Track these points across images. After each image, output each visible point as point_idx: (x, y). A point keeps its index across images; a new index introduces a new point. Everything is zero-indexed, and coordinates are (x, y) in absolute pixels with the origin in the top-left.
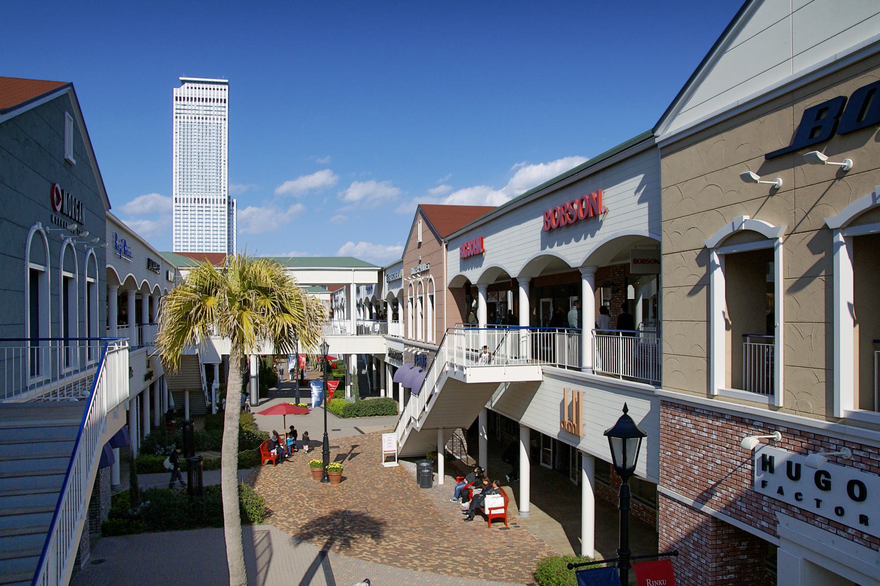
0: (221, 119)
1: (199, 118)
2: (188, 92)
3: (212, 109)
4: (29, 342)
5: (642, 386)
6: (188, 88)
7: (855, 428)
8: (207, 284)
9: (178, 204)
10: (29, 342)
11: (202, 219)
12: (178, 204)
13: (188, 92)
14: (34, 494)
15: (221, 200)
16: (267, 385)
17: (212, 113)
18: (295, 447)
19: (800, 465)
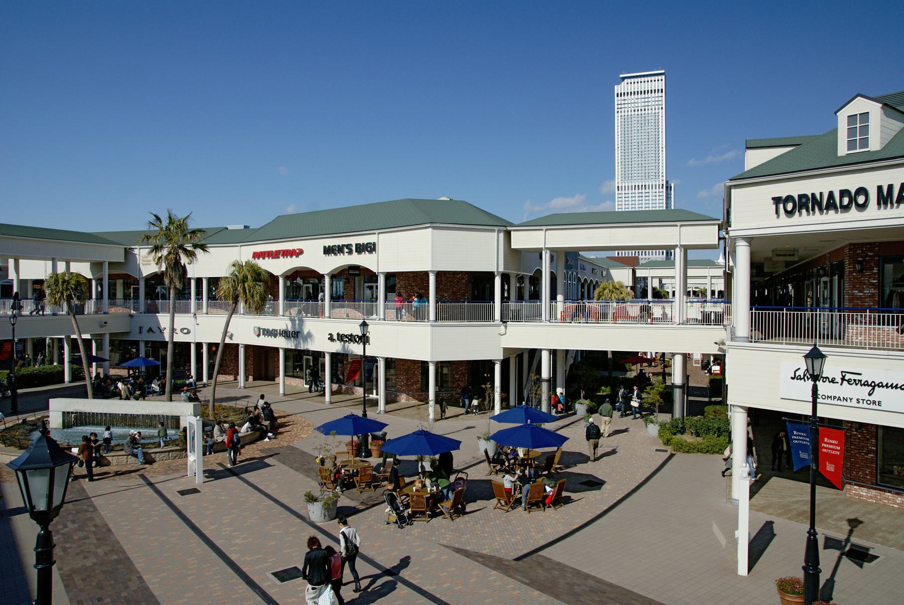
2: (628, 87)
13: (628, 87)
17: (650, 104)
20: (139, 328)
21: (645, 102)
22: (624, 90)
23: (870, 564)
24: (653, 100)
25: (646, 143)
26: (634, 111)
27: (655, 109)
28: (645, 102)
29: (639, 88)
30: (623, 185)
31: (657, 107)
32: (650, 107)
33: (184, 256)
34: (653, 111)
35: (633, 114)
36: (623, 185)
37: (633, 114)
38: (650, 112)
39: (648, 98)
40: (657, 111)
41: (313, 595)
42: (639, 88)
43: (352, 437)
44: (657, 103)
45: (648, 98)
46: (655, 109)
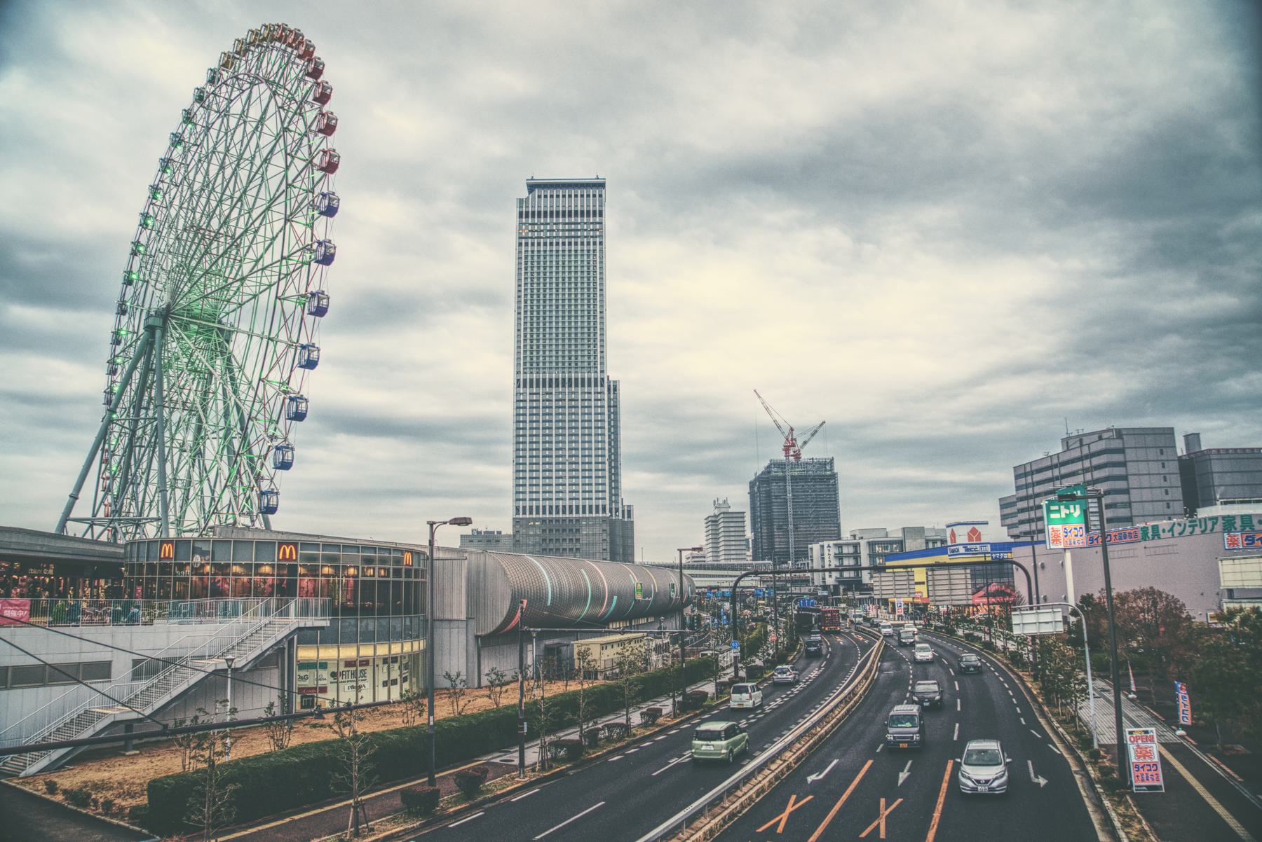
0: (595, 243)
6: (539, 197)
31: (592, 240)
32: (579, 240)
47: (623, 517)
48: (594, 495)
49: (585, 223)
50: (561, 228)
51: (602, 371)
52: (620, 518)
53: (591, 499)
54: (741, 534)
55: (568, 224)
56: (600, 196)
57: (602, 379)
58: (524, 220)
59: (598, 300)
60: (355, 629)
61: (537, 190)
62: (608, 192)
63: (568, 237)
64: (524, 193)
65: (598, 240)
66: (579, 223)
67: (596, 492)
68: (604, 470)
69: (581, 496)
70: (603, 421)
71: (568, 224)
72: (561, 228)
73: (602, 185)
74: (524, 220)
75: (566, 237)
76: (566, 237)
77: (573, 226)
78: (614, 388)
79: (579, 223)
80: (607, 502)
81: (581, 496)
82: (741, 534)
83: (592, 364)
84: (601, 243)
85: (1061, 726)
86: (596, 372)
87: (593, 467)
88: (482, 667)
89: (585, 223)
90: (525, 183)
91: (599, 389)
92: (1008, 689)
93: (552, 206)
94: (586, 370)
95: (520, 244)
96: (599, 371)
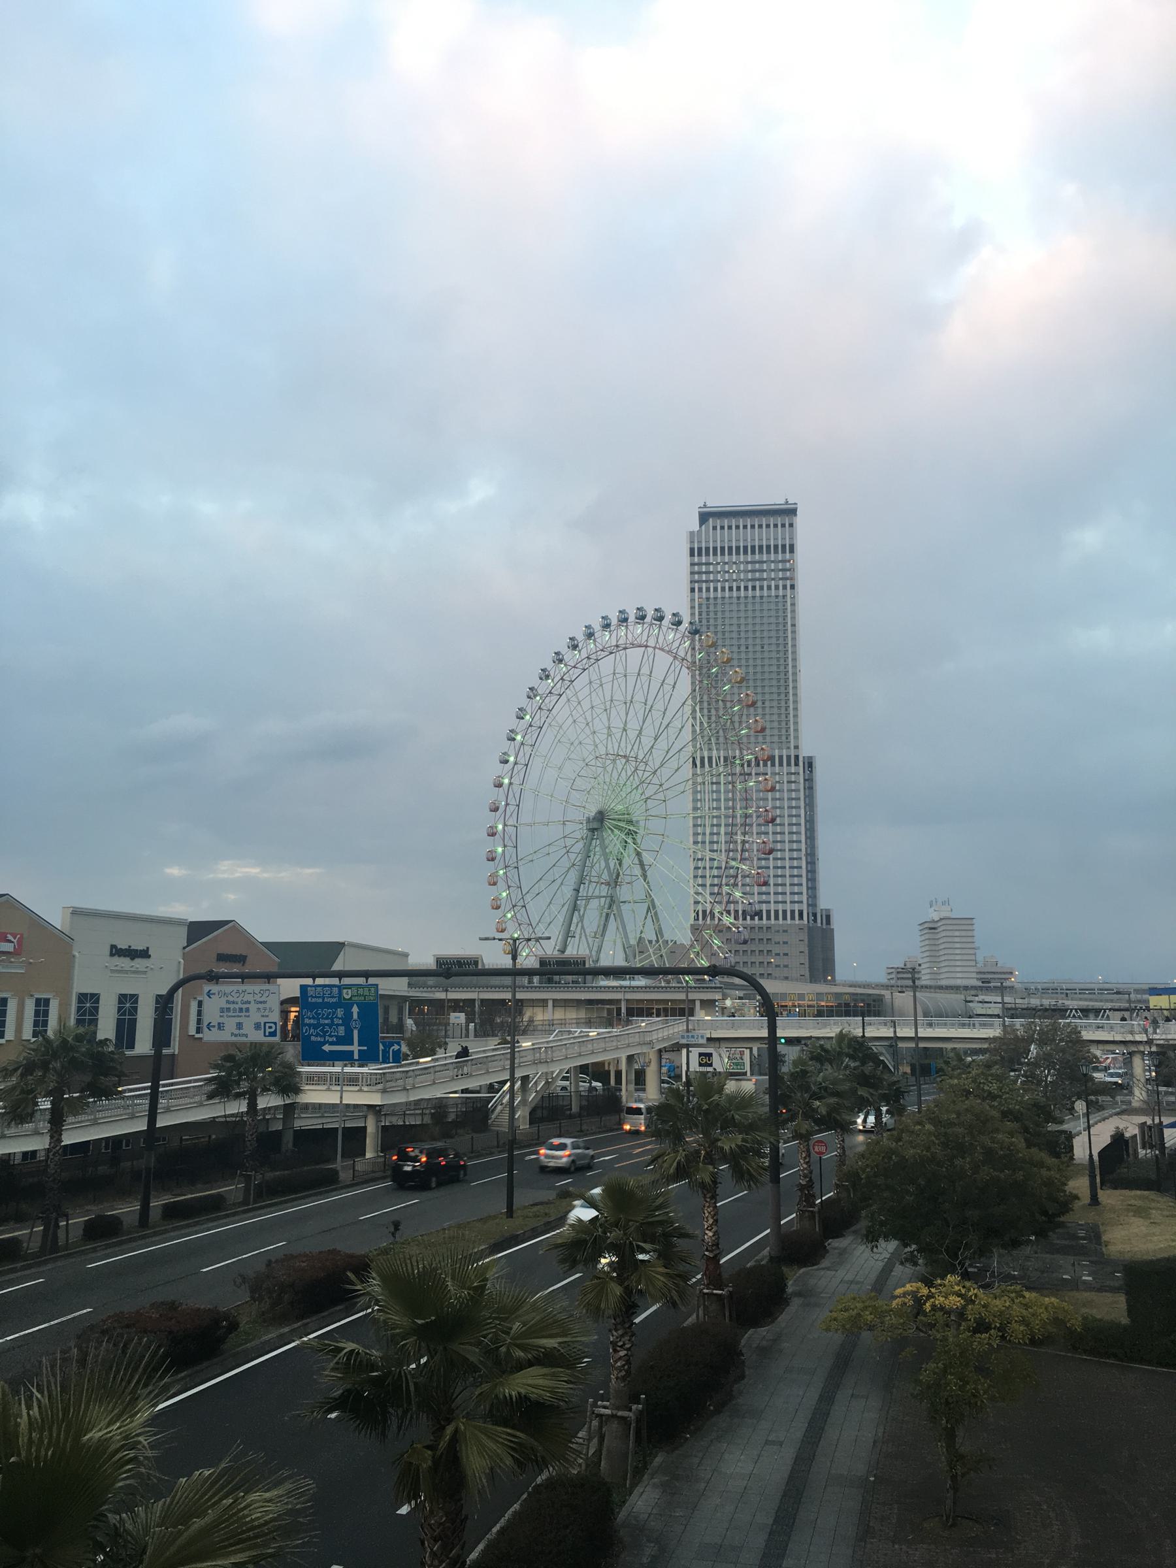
0: (785, 587)
1: (738, 588)
2: (715, 536)
3: (765, 566)
4: (914, 1046)
5: (175, 1028)
6: (715, 528)
7: (13, 971)
8: (1030, 1304)
9: (796, 907)
10: (914, 1046)
11: (790, 850)
12: (796, 907)
13: (715, 536)
14: (1107, 983)
15: (789, 757)
16: (863, 1181)
17: (765, 575)
18: (1081, 1252)
19: (218, 955)
20: (116, 958)
21: (753, 571)
22: (707, 542)
23: (447, 981)
24: (773, 567)
25: (758, 655)
26: (731, 589)
27: (754, 588)
28: (753, 571)
29: (726, 540)
30: (785, 753)
31: (781, 583)
32: (765, 583)
33: (596, 1442)
34: (773, 593)
35: (727, 595)
36: (785, 753)
37: (727, 595)
38: (765, 593)
39: (762, 562)
40: (781, 593)
41: (355, 1425)
42: (726, 540)
43: (341, 1102)
44: (781, 575)
45: (762, 562)
46: (777, 587)
47: (822, 923)
48: (788, 898)
49: (772, 562)
50: (742, 569)
51: (796, 747)
52: (819, 925)
53: (786, 902)
54: (969, 940)
55: (751, 562)
56: (791, 525)
57: (797, 757)
58: (696, 559)
59: (790, 672)
60: (807, 1214)
61: (711, 520)
62: (800, 520)
63: (752, 580)
64: (695, 526)
65: (788, 583)
66: (765, 562)
67: (790, 850)
68: (800, 842)
69: (772, 898)
70: (798, 833)
71: (751, 562)
72: (742, 569)
73: (793, 512)
74: (696, 559)
75: (749, 580)
76: (749, 580)
77: (757, 566)
78: (810, 764)
79: (765, 562)
80: (805, 907)
81: (772, 898)
82: (969, 940)
83: (784, 738)
84: (793, 587)
85: (478, 1251)
86: (789, 748)
87: (787, 846)
88: (431, 978)
89: (772, 562)
90: (698, 510)
91: (793, 769)
92: (373, 1309)
93: (730, 541)
94: (775, 745)
95: (693, 590)
96: (792, 747)
